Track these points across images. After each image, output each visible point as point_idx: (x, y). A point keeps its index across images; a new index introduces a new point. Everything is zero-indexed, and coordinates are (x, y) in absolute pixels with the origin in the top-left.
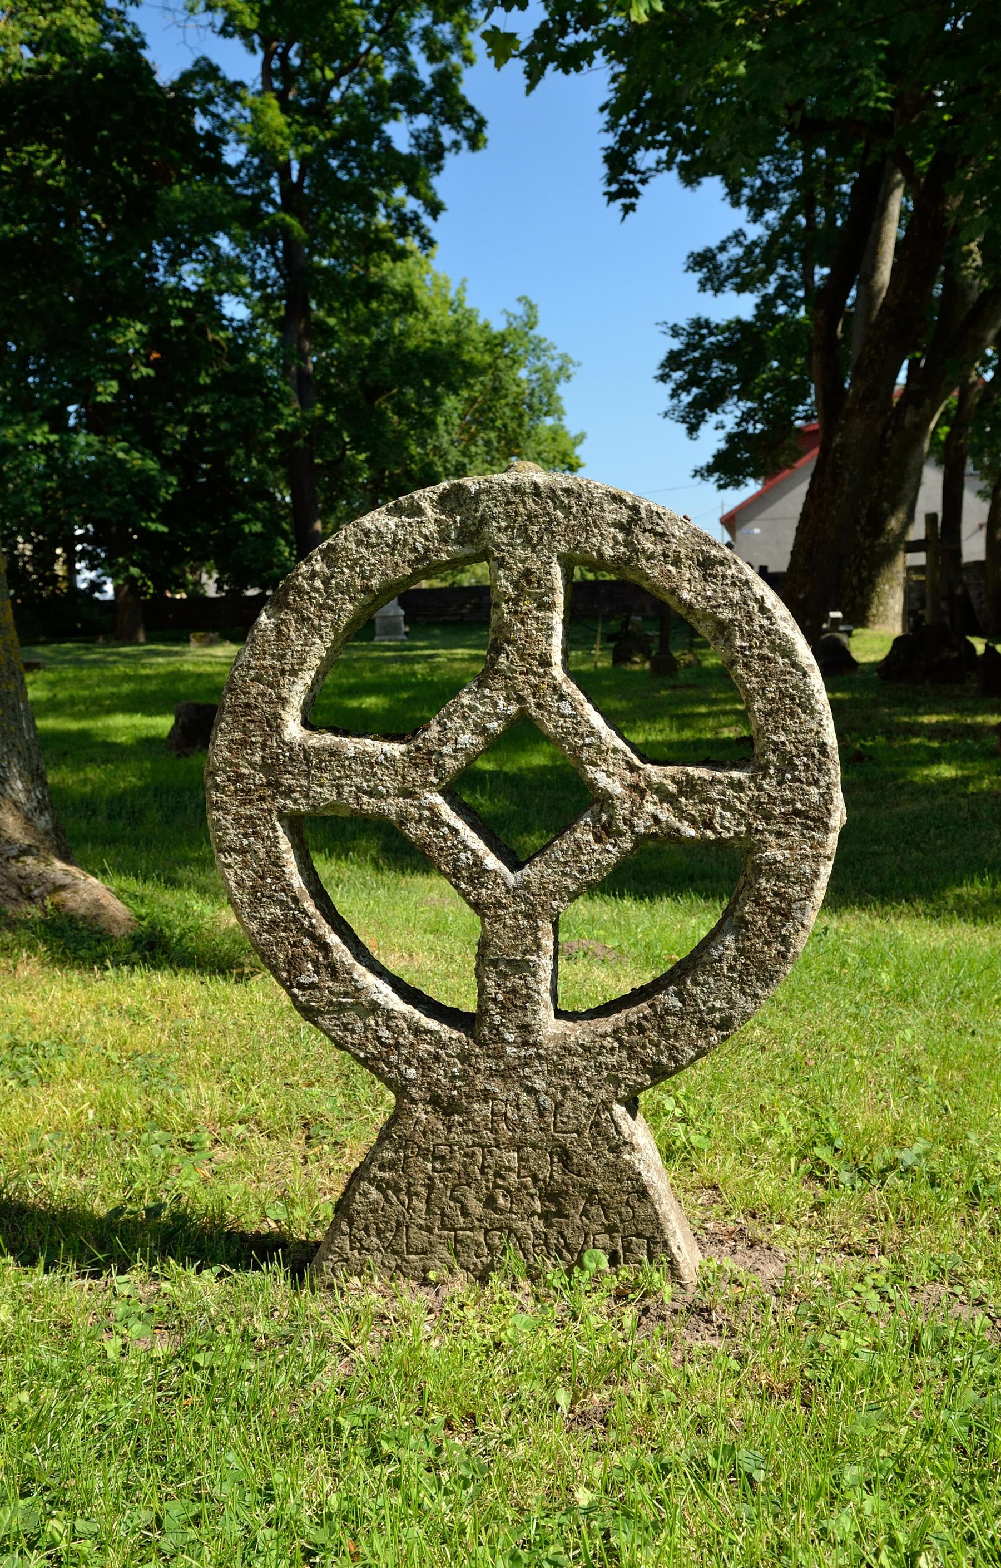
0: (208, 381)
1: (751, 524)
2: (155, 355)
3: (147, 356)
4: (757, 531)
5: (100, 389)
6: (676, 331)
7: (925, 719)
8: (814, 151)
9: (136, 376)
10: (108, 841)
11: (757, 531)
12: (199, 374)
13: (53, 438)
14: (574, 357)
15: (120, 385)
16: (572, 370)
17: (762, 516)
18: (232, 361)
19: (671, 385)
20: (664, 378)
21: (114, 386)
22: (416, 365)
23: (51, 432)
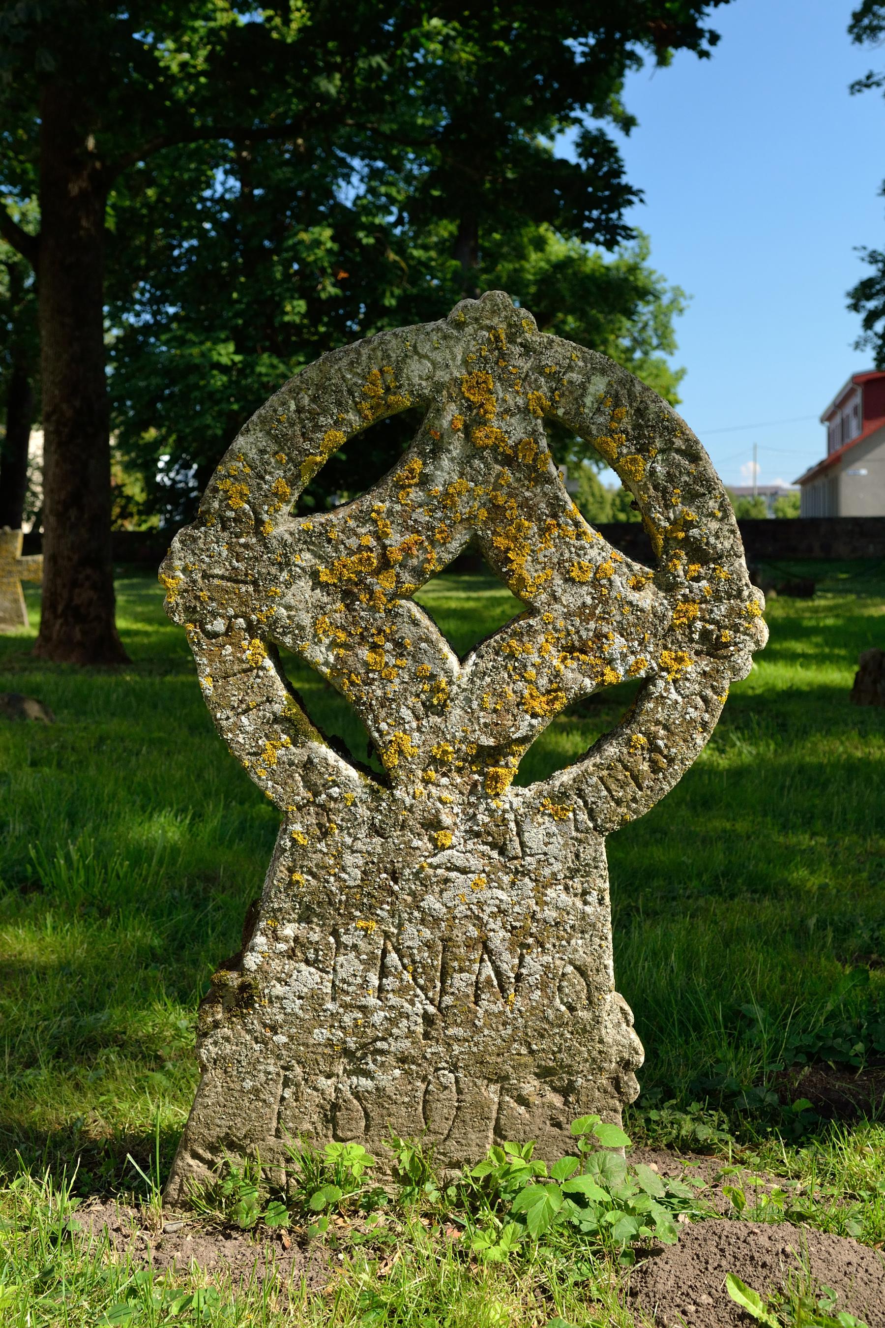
0: (394, 302)
1: (857, 465)
2: (343, 275)
3: (335, 275)
4: (864, 472)
5: (288, 308)
6: (874, 258)
7: (36, 441)
8: (589, 168)
9: (323, 296)
10: (264, 867)
11: (864, 472)
12: (383, 294)
13: (238, 358)
14: (687, 290)
15: (309, 305)
16: (683, 303)
17: (870, 456)
18: (413, 283)
19: (862, 315)
20: (855, 307)
21: (301, 305)
22: (593, 289)
23: (236, 352)
